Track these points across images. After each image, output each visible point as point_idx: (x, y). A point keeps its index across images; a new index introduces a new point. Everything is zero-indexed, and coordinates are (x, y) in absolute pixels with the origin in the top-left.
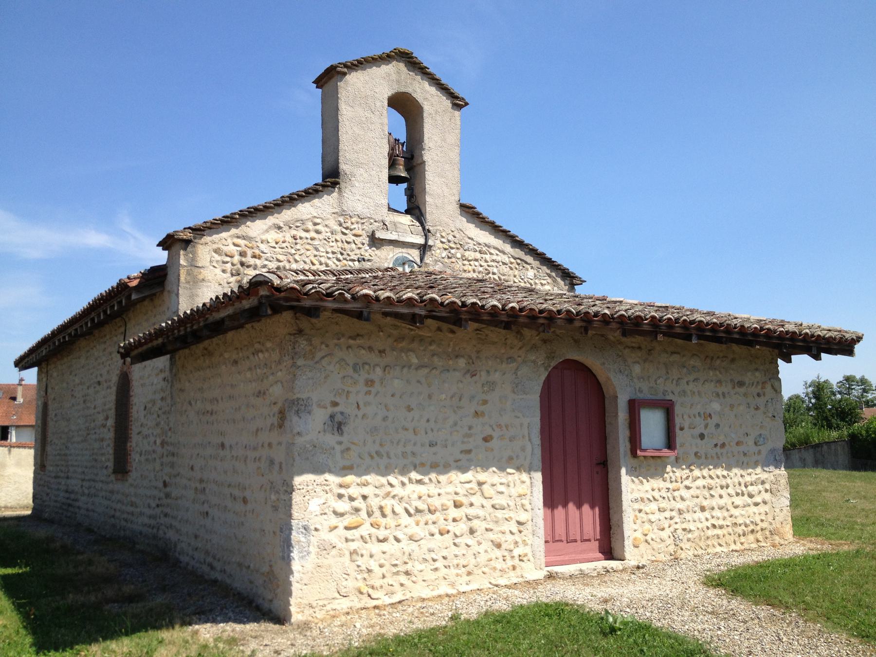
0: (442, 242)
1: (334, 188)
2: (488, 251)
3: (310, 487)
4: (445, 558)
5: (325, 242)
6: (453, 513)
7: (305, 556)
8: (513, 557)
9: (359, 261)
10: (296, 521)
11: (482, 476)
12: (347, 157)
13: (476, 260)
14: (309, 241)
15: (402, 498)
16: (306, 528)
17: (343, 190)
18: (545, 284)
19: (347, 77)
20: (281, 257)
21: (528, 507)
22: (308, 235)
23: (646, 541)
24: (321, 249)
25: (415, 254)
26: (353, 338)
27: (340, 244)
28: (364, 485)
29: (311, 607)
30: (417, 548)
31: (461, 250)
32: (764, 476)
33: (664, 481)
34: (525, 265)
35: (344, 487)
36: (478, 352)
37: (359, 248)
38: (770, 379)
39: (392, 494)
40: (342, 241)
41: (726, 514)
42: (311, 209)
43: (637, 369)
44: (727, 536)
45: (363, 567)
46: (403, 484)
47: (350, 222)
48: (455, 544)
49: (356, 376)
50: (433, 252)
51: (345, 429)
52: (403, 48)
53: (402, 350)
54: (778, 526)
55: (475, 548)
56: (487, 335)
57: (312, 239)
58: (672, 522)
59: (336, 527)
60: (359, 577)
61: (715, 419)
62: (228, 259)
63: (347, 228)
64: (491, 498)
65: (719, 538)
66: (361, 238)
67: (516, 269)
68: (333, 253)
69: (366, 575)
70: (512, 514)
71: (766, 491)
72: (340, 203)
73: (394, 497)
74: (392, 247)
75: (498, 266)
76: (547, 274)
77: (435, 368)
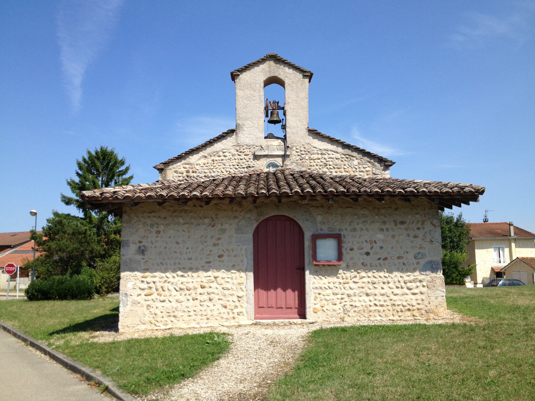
0: (297, 152)
1: (233, 133)
2: (327, 153)
3: (128, 277)
4: (195, 311)
5: (229, 160)
6: (200, 290)
7: (125, 306)
8: (233, 313)
9: (247, 168)
10: (122, 291)
11: (217, 274)
12: (240, 117)
13: (319, 159)
14: (221, 161)
15: (172, 283)
16: (126, 294)
17: (238, 133)
18: (366, 167)
19: (240, 76)
20: (206, 171)
21: (244, 289)
22: (220, 158)
23: (323, 310)
24: (227, 164)
25: (279, 161)
26: (150, 213)
27: (237, 161)
28: (154, 277)
29: (128, 327)
30: (180, 306)
31: (309, 155)
32: (421, 277)
33: (338, 278)
34: (352, 158)
35: (144, 277)
36: (216, 215)
37: (248, 161)
38: (429, 219)
39: (168, 281)
40: (238, 159)
41: (386, 298)
42: (222, 145)
43: (319, 218)
44: (387, 311)
45: (153, 312)
46: (174, 277)
47: (242, 149)
48: (200, 305)
49: (151, 229)
50: (291, 158)
51: (145, 253)
52: (271, 53)
53: (176, 217)
54: (432, 308)
55: (212, 307)
56: (221, 207)
57: (222, 160)
58: (342, 301)
59: (140, 295)
60: (151, 316)
61: (379, 244)
62: (181, 175)
63: (241, 152)
64: (222, 284)
65: (379, 312)
66: (249, 156)
67: (346, 161)
68: (233, 165)
69: (154, 316)
70: (234, 292)
71: (424, 286)
72: (237, 140)
73: (169, 282)
74: (266, 158)
75: (333, 160)
76: (368, 161)
77: (192, 224)
